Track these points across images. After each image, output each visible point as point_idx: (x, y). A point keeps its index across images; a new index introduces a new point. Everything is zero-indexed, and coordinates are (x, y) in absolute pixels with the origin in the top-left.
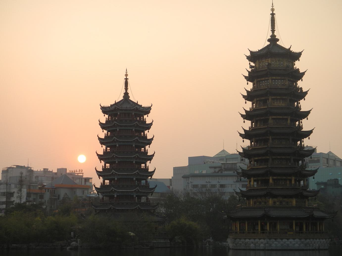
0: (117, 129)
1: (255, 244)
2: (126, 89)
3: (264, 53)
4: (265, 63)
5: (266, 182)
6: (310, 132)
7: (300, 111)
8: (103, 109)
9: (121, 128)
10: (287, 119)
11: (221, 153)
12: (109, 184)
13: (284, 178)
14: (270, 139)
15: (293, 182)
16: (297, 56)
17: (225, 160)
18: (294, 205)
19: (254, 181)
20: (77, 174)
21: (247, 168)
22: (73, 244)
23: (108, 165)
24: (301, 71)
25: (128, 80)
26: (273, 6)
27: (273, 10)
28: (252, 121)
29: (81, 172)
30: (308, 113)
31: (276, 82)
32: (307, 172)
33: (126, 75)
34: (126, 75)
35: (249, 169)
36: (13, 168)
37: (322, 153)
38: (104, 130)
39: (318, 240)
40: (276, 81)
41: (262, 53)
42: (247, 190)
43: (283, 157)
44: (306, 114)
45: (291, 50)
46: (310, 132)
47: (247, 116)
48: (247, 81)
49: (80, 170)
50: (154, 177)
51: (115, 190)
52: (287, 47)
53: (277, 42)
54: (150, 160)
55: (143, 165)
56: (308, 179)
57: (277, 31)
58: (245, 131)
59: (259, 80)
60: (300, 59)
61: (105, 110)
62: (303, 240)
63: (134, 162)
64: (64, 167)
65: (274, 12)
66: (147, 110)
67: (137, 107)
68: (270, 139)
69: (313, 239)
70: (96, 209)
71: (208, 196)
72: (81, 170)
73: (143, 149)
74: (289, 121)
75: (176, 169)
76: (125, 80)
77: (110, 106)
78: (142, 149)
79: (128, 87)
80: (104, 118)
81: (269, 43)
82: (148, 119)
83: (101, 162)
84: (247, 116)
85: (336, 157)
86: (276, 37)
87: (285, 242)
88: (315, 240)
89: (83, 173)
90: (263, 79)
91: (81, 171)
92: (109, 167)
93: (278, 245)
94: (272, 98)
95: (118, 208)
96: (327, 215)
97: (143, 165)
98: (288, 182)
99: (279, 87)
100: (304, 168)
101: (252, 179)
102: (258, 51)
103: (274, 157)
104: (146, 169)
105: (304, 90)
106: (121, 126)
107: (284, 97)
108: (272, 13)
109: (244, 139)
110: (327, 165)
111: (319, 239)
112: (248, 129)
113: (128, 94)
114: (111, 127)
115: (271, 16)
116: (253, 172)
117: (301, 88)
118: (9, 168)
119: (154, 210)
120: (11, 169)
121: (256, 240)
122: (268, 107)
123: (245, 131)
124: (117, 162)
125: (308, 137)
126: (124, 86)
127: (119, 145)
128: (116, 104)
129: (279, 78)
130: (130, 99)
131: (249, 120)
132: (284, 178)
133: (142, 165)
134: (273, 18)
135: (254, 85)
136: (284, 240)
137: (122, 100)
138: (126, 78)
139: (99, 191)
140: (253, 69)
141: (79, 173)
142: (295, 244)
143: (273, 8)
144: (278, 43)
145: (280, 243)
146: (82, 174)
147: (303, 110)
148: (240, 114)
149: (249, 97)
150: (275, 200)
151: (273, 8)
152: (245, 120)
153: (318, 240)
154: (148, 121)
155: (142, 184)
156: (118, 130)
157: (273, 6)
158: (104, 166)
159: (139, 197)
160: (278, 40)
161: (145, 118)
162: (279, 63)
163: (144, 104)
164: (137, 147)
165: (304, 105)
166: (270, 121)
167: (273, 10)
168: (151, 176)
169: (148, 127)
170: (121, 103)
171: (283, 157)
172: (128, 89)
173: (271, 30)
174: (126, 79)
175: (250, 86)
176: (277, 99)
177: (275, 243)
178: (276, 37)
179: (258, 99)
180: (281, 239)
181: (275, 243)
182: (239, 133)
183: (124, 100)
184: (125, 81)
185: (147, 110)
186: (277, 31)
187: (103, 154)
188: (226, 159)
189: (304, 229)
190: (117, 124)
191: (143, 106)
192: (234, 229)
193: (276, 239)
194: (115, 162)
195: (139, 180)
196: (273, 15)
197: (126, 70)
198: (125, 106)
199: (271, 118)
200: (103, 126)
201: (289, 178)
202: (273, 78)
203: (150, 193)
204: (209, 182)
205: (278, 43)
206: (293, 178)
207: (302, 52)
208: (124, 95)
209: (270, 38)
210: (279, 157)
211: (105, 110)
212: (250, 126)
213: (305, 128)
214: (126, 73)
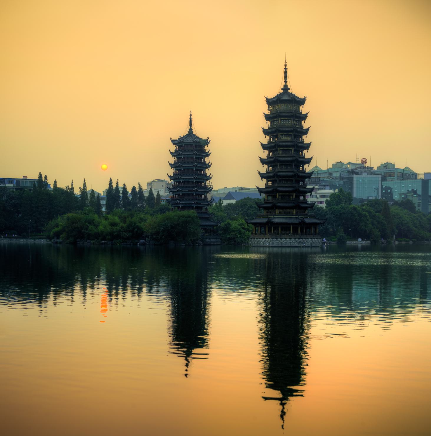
0: (182, 157)
2: (191, 126)
4: (280, 107)
5: (274, 197)
9: (185, 156)
13: (288, 194)
16: (302, 102)
17: (317, 175)
22: (141, 241)
26: (286, 63)
31: (287, 122)
36: (155, 181)
39: (310, 240)
40: (285, 121)
43: (287, 179)
51: (179, 203)
59: (273, 120)
61: (174, 142)
62: (297, 240)
63: (194, 182)
64: (132, 187)
65: (287, 67)
74: (293, 152)
85: (411, 172)
90: (275, 120)
93: (283, 243)
94: (280, 134)
96: (318, 221)
102: (272, 98)
103: (281, 179)
106: (185, 155)
107: (290, 133)
110: (402, 178)
111: (311, 239)
113: (192, 130)
118: (153, 181)
120: (153, 183)
121: (264, 239)
126: (284, 79)
129: (287, 119)
132: (288, 194)
138: (286, 68)
142: (291, 242)
144: (289, 91)
150: (281, 210)
153: (310, 240)
156: (183, 157)
160: (289, 89)
162: (287, 107)
164: (197, 170)
169: (307, 146)
171: (287, 179)
172: (287, 81)
174: (191, 118)
176: (285, 135)
181: (276, 241)
188: (318, 174)
189: (299, 232)
191: (299, 98)
192: (332, 244)
193: (277, 239)
196: (286, 69)
198: (189, 140)
202: (282, 119)
205: (289, 91)
206: (294, 194)
211: (174, 142)
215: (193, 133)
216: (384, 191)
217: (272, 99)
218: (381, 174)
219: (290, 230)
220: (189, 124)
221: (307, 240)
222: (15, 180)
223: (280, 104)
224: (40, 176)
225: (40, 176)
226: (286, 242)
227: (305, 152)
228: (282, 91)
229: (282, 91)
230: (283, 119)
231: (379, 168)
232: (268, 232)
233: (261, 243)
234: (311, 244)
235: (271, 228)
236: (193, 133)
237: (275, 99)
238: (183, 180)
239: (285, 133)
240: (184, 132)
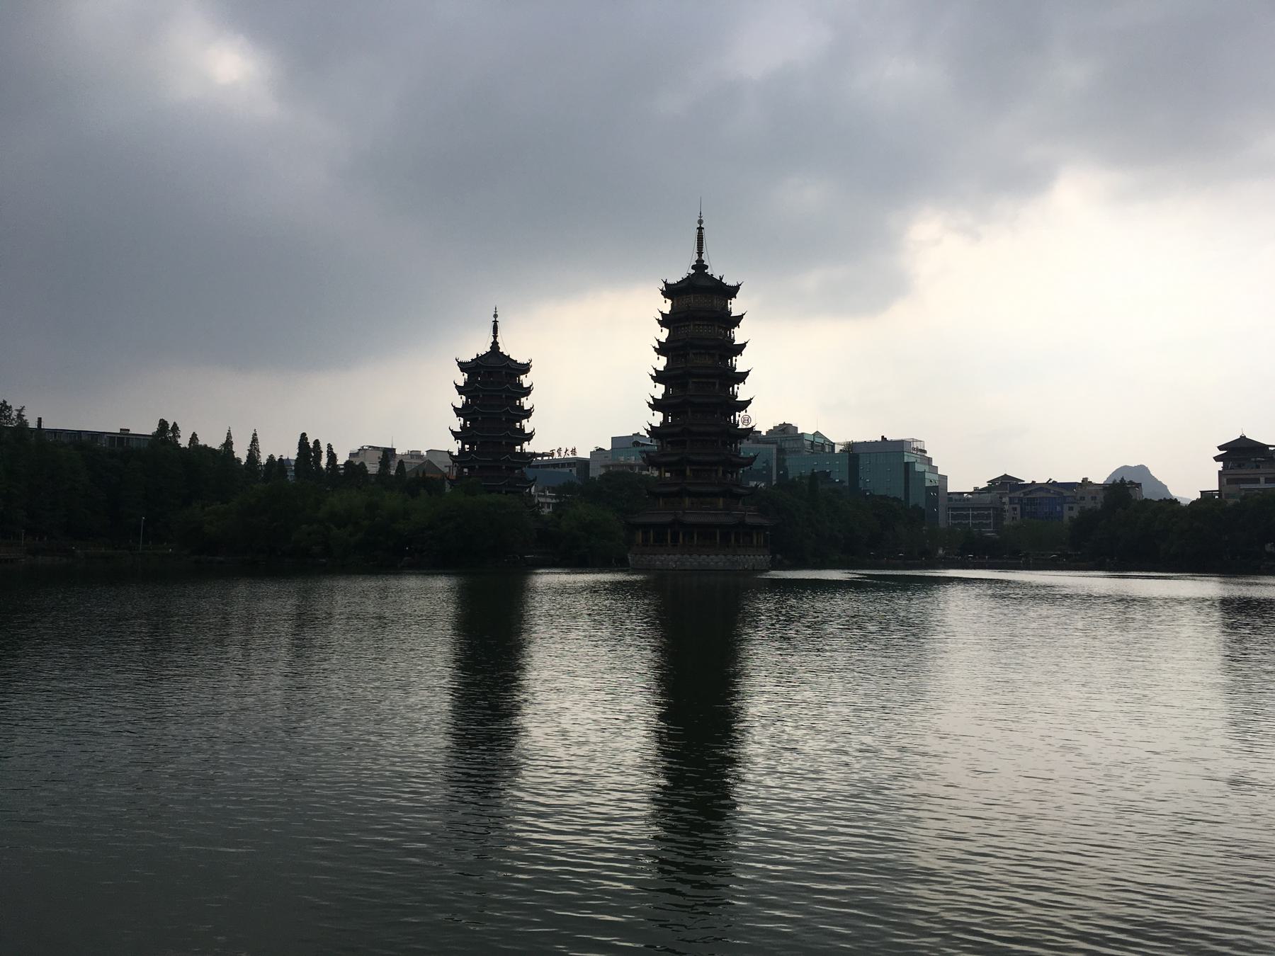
1: (675, 562)
4: (691, 300)
10: (714, 384)
27: (700, 222)
32: (741, 460)
44: (742, 377)
47: (658, 377)
55: (518, 448)
59: (676, 325)
61: (463, 366)
66: (525, 368)
73: (518, 424)
74: (717, 386)
80: (461, 378)
82: (525, 381)
84: (658, 377)
97: (518, 448)
101: (663, 469)
106: (485, 391)
112: (660, 397)
114: (471, 391)
116: (664, 459)
120: (361, 452)
128: (479, 358)
136: (711, 557)
149: (662, 349)
152: (660, 356)
160: (706, 267)
163: (522, 360)
165: (740, 364)
169: (527, 392)
175: (664, 335)
185: (525, 368)
189: (681, 540)
191: (518, 362)
193: (690, 555)
196: (700, 229)
200: (461, 390)
206: (721, 469)
211: (463, 366)
213: (742, 397)
215: (501, 351)
216: (781, 472)
218: (777, 443)
222: (106, 435)
224: (1217, 459)
225: (1217, 459)
227: (524, 422)
229: (692, 272)
230: (698, 323)
231: (770, 432)
232: (671, 542)
233: (658, 563)
234: (754, 566)
235: (679, 534)
236: (501, 351)
239: (703, 351)
240: (484, 348)
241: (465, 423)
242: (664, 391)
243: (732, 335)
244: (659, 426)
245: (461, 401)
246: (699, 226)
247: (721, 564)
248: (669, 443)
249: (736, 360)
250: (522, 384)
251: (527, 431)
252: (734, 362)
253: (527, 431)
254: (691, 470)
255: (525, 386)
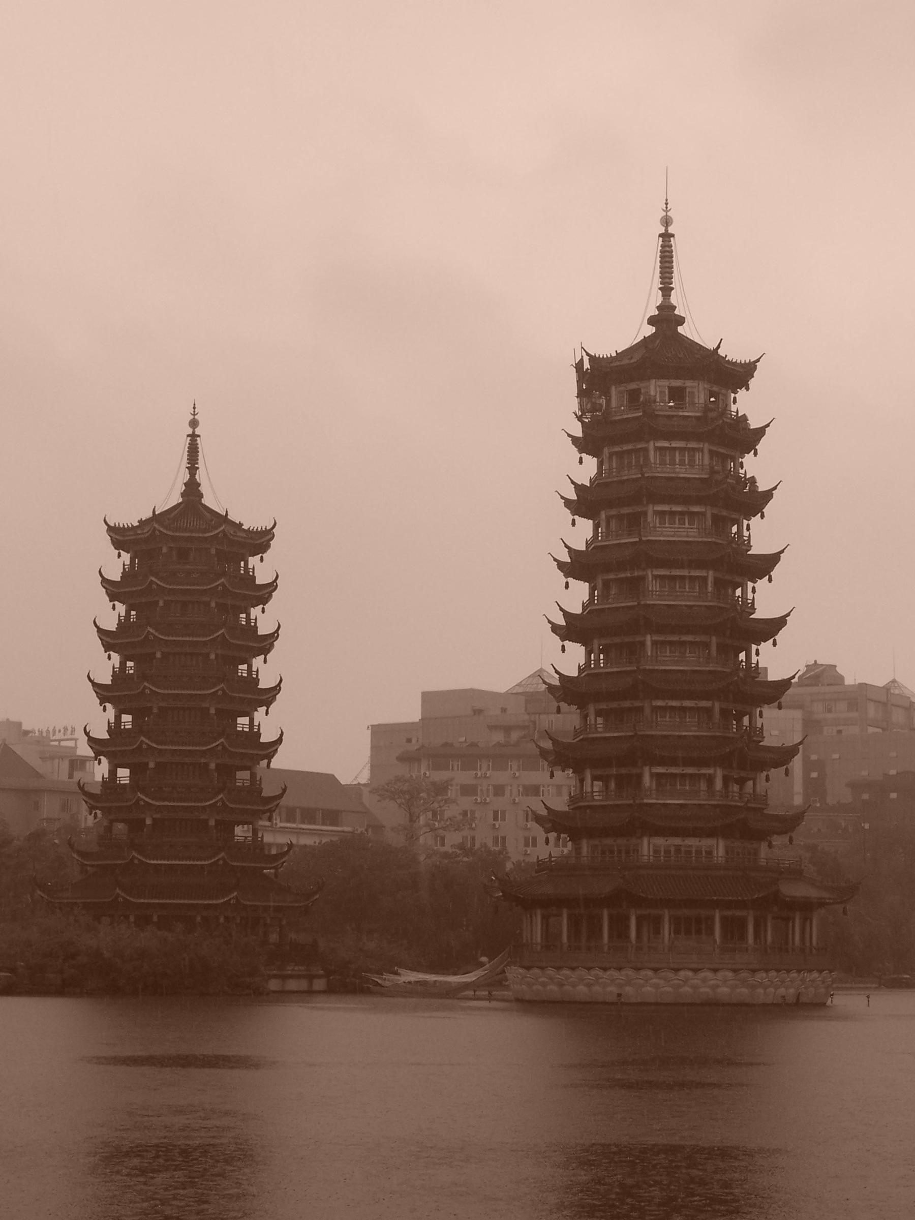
2: (193, 468)
3: (632, 361)
6: (779, 623)
7: (749, 553)
8: (113, 535)
11: (531, 679)
12: (128, 782)
14: (649, 643)
15: (719, 784)
18: (720, 859)
19: (595, 778)
20: (56, 743)
21: (574, 736)
23: (127, 718)
24: (754, 424)
25: (198, 439)
27: (667, 221)
28: (592, 585)
29: (70, 737)
30: (772, 560)
33: (194, 423)
34: (194, 423)
35: (578, 739)
37: (866, 684)
38: (116, 603)
39: (795, 975)
41: (626, 361)
42: (571, 807)
45: (721, 352)
46: (779, 623)
48: (581, 451)
49: (66, 729)
50: (276, 763)
52: (710, 344)
53: (679, 327)
54: (268, 703)
56: (769, 773)
57: (679, 295)
58: (566, 614)
60: (752, 383)
62: (744, 974)
65: (671, 230)
67: (223, 531)
68: (649, 643)
69: (778, 971)
70: (86, 865)
71: (461, 828)
72: (70, 729)
73: (245, 667)
75: (380, 733)
76: (189, 438)
77: (136, 524)
78: (240, 667)
79: (197, 464)
81: (650, 330)
83: (105, 710)
86: (676, 312)
87: (686, 981)
88: (783, 974)
89: (76, 740)
91: (69, 732)
92: (130, 727)
93: (702, 990)
95: (155, 862)
97: (243, 721)
98: (703, 786)
99: (679, 473)
100: (754, 741)
102: (614, 354)
104: (254, 735)
105: (762, 487)
107: (696, 509)
108: (663, 231)
109: (567, 643)
111: (799, 971)
113: (199, 485)
115: (660, 243)
117: (753, 480)
119: (276, 868)
122: (640, 540)
123: (566, 614)
124: (155, 710)
125: (771, 640)
127: (163, 653)
130: (203, 502)
131: (585, 581)
132: (690, 770)
133: (238, 719)
134: (667, 249)
135: (600, 465)
136: (702, 975)
137: (179, 505)
139: (95, 804)
140: (598, 413)
141: (63, 737)
142: (718, 986)
143: (667, 215)
144: (680, 329)
145: (672, 982)
146: (58, 742)
147: (758, 548)
148: (555, 560)
151: (667, 215)
152: (570, 580)
153: (794, 974)
154: (262, 577)
155: (238, 784)
157: (667, 208)
158: (112, 720)
159: (227, 827)
160: (681, 321)
161: (250, 566)
166: (653, 585)
167: (667, 223)
168: (270, 757)
169: (265, 644)
170: (173, 514)
172: (673, 289)
173: (660, 289)
174: (194, 437)
177: (655, 981)
178: (676, 312)
179: (613, 512)
180: (673, 969)
182: (550, 622)
183: (182, 505)
184: (188, 441)
186: (679, 295)
187: (110, 683)
190: (158, 585)
191: (245, 527)
194: (151, 708)
195: (227, 771)
196: (666, 237)
197: (194, 408)
199: (650, 576)
200: (114, 591)
201: (704, 771)
203: (264, 812)
204: (486, 777)
205: (680, 329)
207: (758, 360)
208: (184, 488)
209: (657, 313)
210: (674, 703)
212: (586, 598)
214: (194, 415)
217: (611, 359)
219: (711, 932)
220: (185, 463)
221: (582, 972)
223: (653, 381)
226: (544, 985)
228: (650, 330)
229: (650, 330)
237: (637, 357)
238: (161, 704)
241: (123, 664)
242: (580, 423)
243: (746, 533)
244: (576, 674)
245: (110, 663)
246: (663, 231)
247: (724, 990)
248: (599, 713)
249: (754, 591)
250: (256, 627)
251: (265, 683)
252: (750, 596)
253: (265, 683)
254: (652, 775)
255: (262, 631)
